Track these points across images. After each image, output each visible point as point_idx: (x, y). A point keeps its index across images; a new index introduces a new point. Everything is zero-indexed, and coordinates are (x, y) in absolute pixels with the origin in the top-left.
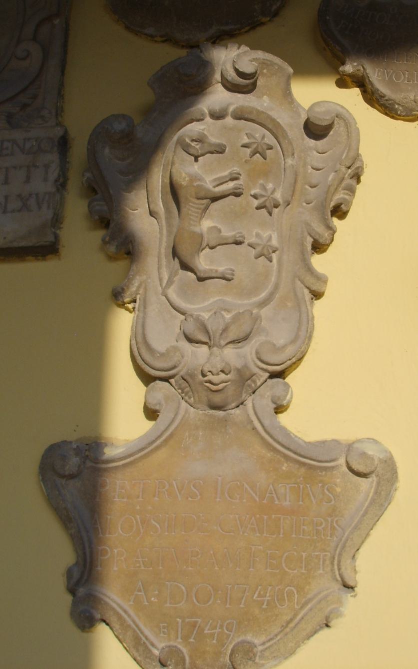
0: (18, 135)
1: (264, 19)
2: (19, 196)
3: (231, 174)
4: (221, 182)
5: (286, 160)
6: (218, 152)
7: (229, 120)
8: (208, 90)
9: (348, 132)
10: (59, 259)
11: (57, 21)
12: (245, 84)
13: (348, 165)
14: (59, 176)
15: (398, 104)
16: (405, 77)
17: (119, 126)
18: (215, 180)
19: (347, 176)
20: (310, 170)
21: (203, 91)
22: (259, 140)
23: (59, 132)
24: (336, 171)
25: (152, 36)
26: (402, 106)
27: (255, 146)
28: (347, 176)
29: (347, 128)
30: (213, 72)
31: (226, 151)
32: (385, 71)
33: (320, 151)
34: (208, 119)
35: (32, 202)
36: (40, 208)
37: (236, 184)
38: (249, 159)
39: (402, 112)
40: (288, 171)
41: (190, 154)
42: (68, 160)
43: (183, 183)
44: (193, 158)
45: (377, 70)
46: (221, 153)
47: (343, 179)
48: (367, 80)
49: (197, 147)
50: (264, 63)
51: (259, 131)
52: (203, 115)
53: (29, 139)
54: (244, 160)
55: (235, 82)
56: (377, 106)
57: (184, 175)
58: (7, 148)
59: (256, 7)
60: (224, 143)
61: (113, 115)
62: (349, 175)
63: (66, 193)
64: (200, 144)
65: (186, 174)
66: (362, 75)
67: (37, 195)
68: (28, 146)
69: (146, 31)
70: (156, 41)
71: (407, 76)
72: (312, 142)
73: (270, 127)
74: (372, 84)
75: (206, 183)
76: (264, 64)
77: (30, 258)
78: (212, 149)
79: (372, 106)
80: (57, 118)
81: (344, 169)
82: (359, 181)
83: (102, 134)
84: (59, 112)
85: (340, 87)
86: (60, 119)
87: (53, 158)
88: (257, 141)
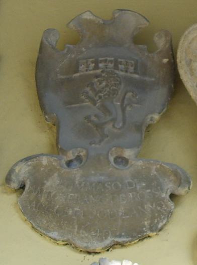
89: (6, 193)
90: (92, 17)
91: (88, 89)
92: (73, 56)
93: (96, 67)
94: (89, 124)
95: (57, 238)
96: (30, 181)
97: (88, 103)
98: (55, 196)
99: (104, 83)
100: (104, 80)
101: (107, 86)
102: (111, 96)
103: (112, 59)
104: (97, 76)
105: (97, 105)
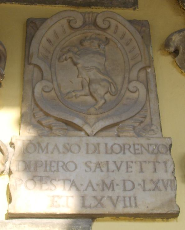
0: (143, 141)
2: (152, 180)
10: (177, 221)
11: (149, 70)
35: (160, 185)
36: (166, 189)
53: (151, 145)
68: (151, 148)
77: (160, 219)
89: (163, 55)
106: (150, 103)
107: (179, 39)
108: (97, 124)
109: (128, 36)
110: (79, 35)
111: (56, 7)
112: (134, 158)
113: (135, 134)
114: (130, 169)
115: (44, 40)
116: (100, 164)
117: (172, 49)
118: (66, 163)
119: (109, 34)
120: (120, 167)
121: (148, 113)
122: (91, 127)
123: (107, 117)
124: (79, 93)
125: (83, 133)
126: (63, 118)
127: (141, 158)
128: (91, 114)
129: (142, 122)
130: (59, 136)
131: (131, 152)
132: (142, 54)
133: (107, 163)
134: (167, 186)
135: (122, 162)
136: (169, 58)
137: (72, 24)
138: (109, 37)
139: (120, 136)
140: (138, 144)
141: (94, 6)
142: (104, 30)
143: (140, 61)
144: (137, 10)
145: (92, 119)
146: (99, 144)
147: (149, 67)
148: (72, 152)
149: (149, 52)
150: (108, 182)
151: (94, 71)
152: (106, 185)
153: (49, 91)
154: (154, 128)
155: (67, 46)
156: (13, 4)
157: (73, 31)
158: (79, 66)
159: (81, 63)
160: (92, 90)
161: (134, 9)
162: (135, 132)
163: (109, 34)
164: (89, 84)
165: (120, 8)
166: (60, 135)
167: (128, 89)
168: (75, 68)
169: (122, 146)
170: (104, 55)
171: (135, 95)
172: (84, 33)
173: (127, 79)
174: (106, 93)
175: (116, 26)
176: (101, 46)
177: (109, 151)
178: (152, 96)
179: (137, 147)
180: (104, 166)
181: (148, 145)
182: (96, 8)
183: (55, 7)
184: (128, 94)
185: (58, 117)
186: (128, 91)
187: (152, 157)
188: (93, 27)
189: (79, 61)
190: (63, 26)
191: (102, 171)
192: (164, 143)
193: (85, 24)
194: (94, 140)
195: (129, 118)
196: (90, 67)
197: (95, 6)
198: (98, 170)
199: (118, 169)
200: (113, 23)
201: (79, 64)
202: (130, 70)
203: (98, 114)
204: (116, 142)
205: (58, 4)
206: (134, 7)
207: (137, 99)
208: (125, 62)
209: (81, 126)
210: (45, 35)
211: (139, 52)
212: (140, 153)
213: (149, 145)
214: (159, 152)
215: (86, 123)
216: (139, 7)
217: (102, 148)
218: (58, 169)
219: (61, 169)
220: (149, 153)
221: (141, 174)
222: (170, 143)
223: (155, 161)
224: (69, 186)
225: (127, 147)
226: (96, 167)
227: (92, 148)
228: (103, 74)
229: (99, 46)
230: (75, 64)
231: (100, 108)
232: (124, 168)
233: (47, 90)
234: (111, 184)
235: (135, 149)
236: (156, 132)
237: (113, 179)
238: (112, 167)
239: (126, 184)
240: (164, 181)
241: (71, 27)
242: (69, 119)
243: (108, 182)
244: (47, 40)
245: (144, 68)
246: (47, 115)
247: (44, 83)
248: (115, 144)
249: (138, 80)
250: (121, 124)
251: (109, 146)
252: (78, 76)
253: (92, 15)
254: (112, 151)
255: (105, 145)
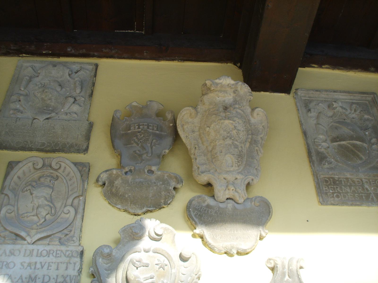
0: (63, 248)
1: (165, 206)
2: (63, 276)
3: (151, 276)
4: (147, 279)
5: (172, 270)
6: (146, 266)
7: (151, 253)
8: (143, 239)
9: (197, 260)
11: (81, 198)
12: (157, 238)
13: (196, 274)
14: (80, 268)
15: (216, 248)
16: (219, 237)
17: (107, 251)
18: (144, 278)
19: (195, 278)
20: (181, 275)
21: (141, 239)
22: (162, 262)
23: (80, 249)
24: (191, 277)
25: (119, 209)
26: (218, 248)
27: (161, 265)
28: (195, 278)
29: (197, 259)
30: (145, 231)
31: (149, 266)
32: (212, 233)
33: (185, 267)
34: (143, 251)
37: (152, 281)
38: (158, 270)
39: (217, 251)
40: (172, 275)
41: (135, 266)
42: (83, 260)
43: (132, 279)
44: (136, 268)
45: (208, 233)
46: (147, 267)
47: (194, 279)
48: (204, 237)
49: (138, 264)
50: (165, 229)
51: (162, 258)
52: (141, 250)
53: (68, 251)
54: (156, 270)
55: (154, 237)
56: (207, 247)
57: (132, 275)
58: (58, 254)
59: (162, 201)
60: (149, 263)
61: (104, 245)
62: (196, 278)
63: (81, 275)
64: (139, 263)
65: (133, 275)
66: (202, 234)
67: (70, 276)
68: (67, 253)
69: (117, 206)
70: (121, 211)
71: (220, 236)
72: (182, 263)
73: (167, 256)
74: (206, 239)
75: (141, 279)
76: (165, 229)
78: (144, 265)
79: (206, 247)
80: (79, 241)
81: (194, 275)
82: (199, 279)
83: (99, 252)
84: (80, 238)
85: (193, 237)
86: (80, 242)
87: (78, 260)
88: (161, 263)
90: (137, 104)
91: (135, 138)
92: (128, 123)
93: (139, 128)
94: (136, 155)
95: (121, 208)
96: (108, 182)
97: (135, 145)
98: (119, 188)
99: (142, 135)
100: (142, 134)
101: (144, 137)
102: (146, 141)
103: (146, 124)
104: (139, 132)
105: (139, 146)
106: (58, 233)
107: (106, 176)
108: (35, 236)
109: (72, 174)
110: (39, 173)
111: (33, 153)
112: (54, 260)
113: (59, 243)
114: (50, 268)
115: (16, 177)
116: (31, 264)
117: (101, 183)
118: (9, 262)
119: (59, 173)
120: (44, 266)
121: (74, 228)
122: (31, 238)
123: (43, 232)
124: (29, 214)
125: (26, 242)
126: (14, 232)
127: (59, 260)
128: (33, 229)
129: (67, 235)
130: (9, 244)
131: (53, 256)
132: (79, 186)
133: (36, 263)
134: (72, 280)
135: (46, 262)
136: (100, 189)
137: (35, 166)
138: (59, 175)
139: (50, 244)
140: (59, 250)
141: (57, 152)
142: (56, 170)
143: (76, 192)
144: (87, 154)
145: (33, 232)
146: (33, 250)
147: (82, 196)
148: (14, 255)
149: (84, 185)
150: (33, 276)
151: (43, 199)
152: (31, 278)
153: (10, 212)
154: (74, 239)
155: (30, 181)
156: (3, 150)
157: (36, 171)
158: (34, 195)
159: (35, 192)
160: (37, 213)
161: (85, 154)
162: (60, 242)
163: (59, 173)
164: (37, 208)
165: (74, 153)
166: (10, 243)
167: (63, 211)
168: (31, 196)
169: (48, 251)
170: (53, 188)
171: (68, 216)
172: (42, 172)
173: (64, 205)
174: (47, 215)
175: (65, 167)
176: (52, 181)
177: (39, 255)
178: (79, 216)
179: (58, 252)
180: (33, 265)
181: (66, 251)
182: (59, 153)
183: (31, 152)
184: (63, 215)
185: (12, 231)
186: (63, 213)
187: (65, 259)
188: (49, 168)
189: (34, 192)
190: (29, 167)
191: (31, 269)
192: (77, 250)
193: (44, 165)
194: (31, 247)
195: (58, 232)
196: (41, 196)
197: (58, 152)
198: (29, 268)
199: (42, 267)
200: (63, 165)
201: (34, 194)
202: (68, 198)
203: (38, 229)
204: (46, 248)
205: (34, 151)
206: (84, 153)
207: (68, 218)
208: (65, 193)
209: (25, 237)
210: (18, 172)
211: (77, 186)
212: (60, 256)
213: (67, 252)
214: (72, 256)
215: (29, 235)
216: (89, 152)
217: (35, 253)
218: (2, 267)
219: (4, 267)
220: (65, 256)
221: (57, 271)
222: (81, 249)
223: (68, 262)
224: (7, 278)
225: (52, 252)
226: (28, 266)
227: (28, 252)
228: (48, 201)
229: (50, 181)
230: (32, 194)
231: (41, 224)
232: (46, 267)
233: (10, 211)
234: (35, 278)
235: (56, 254)
236: (75, 242)
237: (37, 274)
238: (38, 266)
239: (45, 278)
240: (71, 276)
241: (35, 169)
242: (18, 232)
243: (33, 276)
244: (18, 177)
245: (78, 197)
246: (6, 229)
247: (9, 207)
248: (44, 250)
249: (72, 205)
250: (52, 236)
251: (40, 251)
252: (31, 203)
253: (50, 159)
254: (41, 255)
255: (37, 250)
